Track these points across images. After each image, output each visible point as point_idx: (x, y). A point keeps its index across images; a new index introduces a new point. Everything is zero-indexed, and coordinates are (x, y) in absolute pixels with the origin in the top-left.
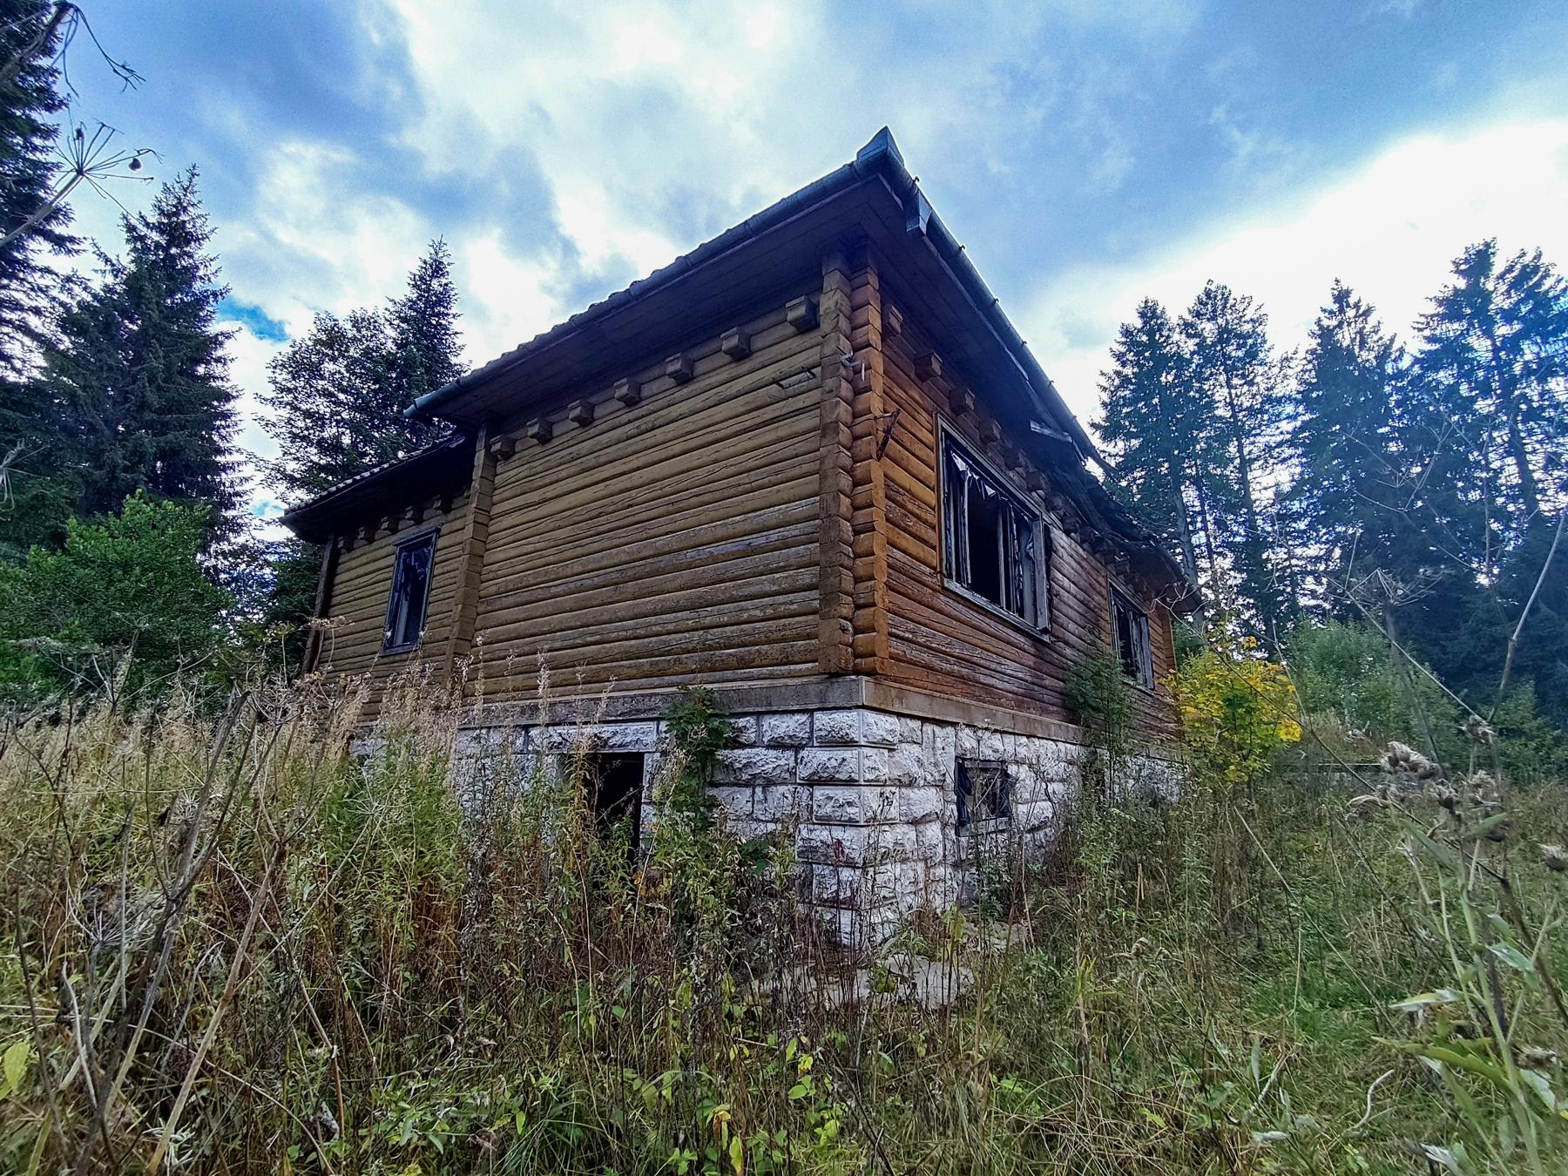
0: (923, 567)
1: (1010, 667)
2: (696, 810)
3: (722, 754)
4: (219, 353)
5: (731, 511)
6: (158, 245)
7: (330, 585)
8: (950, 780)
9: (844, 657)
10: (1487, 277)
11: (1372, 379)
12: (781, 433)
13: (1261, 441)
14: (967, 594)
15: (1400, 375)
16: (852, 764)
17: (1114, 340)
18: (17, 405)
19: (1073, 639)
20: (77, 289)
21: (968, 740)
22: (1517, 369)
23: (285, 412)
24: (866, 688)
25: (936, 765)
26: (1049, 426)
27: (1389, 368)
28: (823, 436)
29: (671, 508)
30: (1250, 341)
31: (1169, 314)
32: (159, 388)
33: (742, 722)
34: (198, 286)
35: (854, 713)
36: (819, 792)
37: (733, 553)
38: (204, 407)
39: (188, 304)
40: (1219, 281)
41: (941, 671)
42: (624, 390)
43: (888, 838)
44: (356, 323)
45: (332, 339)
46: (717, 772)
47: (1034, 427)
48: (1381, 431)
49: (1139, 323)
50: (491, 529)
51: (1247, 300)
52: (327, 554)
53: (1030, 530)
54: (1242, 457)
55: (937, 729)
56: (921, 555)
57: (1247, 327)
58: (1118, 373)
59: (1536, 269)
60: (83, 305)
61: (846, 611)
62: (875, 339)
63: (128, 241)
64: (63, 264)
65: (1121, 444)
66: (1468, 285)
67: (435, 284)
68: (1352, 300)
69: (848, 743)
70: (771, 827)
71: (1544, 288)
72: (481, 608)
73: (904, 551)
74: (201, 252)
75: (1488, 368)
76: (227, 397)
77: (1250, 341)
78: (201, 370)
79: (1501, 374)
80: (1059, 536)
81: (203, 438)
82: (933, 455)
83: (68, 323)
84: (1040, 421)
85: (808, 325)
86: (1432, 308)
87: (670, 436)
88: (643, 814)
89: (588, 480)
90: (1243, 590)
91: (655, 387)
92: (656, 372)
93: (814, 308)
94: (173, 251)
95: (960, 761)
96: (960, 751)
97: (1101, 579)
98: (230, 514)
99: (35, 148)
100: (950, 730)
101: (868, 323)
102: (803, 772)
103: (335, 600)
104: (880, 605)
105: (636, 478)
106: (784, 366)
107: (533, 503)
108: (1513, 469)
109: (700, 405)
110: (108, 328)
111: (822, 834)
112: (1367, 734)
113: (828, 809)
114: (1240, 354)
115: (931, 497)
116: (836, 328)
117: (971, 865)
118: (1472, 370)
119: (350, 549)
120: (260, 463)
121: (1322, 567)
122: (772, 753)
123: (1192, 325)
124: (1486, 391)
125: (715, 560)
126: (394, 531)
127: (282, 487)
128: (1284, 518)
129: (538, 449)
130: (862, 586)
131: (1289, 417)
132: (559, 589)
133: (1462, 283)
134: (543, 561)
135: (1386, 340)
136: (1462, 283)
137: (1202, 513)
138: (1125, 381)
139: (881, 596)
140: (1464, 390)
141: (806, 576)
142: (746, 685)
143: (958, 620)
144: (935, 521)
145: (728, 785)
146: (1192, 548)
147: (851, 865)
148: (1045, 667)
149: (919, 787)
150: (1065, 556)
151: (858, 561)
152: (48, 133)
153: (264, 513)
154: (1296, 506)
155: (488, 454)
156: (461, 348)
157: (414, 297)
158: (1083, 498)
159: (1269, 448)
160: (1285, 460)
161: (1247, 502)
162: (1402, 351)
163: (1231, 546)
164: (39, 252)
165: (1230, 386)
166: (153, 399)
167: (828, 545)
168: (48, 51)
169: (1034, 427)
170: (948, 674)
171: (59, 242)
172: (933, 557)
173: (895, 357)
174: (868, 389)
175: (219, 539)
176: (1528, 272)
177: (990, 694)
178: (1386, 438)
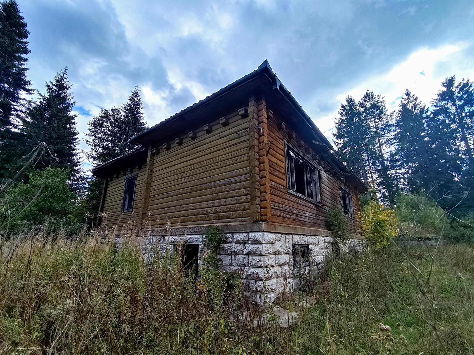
0: (281, 186)
1: (309, 214)
2: (214, 263)
3: (222, 245)
4: (73, 121)
5: (224, 171)
7: (106, 191)
8: (291, 251)
9: (258, 216)
10: (452, 87)
11: (418, 118)
12: (237, 148)
13: (385, 138)
14: (295, 194)
15: (427, 117)
17: (339, 109)
18: (15, 139)
19: (328, 204)
20: (33, 104)
21: (296, 238)
22: (464, 114)
23: (92, 138)
24: (264, 225)
25: (286, 247)
26: (318, 141)
27: (424, 115)
28: (250, 150)
29: (206, 170)
30: (381, 108)
32: (56, 132)
33: (228, 235)
34: (68, 101)
35: (261, 233)
36: (251, 258)
37: (224, 184)
38: (69, 137)
39: (65, 107)
40: (371, 90)
41: (287, 218)
42: (191, 135)
43: (272, 270)
44: (113, 111)
45: (106, 116)
46: (220, 251)
47: (314, 142)
48: (422, 134)
49: (346, 104)
50: (153, 176)
52: (105, 182)
53: (314, 172)
55: (286, 236)
56: (281, 183)
57: (380, 104)
58: (341, 119)
59: (468, 84)
60: (34, 108)
61: (258, 202)
62: (265, 120)
63: (47, 90)
64: (29, 97)
65: (342, 140)
66: (447, 90)
67: (136, 99)
68: (411, 95)
69: (259, 242)
70: (237, 268)
71: (471, 90)
72: (150, 199)
73: (275, 182)
74: (68, 92)
75: (454, 115)
76: (76, 134)
77: (381, 108)
78: (68, 126)
79: (458, 116)
80: (323, 174)
81: (68, 146)
82: (283, 152)
83: (30, 114)
84: (315, 140)
85: (245, 116)
86: (436, 97)
87: (205, 148)
88: (199, 263)
89: (181, 161)
90: (382, 183)
91: (200, 134)
92: (201, 129)
93: (246, 111)
94: (60, 92)
95: (294, 245)
96: (294, 242)
97: (336, 185)
98: (76, 168)
100: (290, 236)
101: (263, 115)
102: (246, 251)
103: (107, 196)
104: (268, 200)
105: (195, 161)
106: (238, 128)
107: (166, 167)
108: (464, 145)
109: (214, 139)
110: (41, 115)
111: (252, 270)
112: (422, 228)
113: (253, 263)
115: (283, 165)
116: (253, 117)
117: (298, 277)
118: (449, 115)
119: (111, 180)
120: (85, 153)
121: (406, 176)
122: (237, 245)
123: (362, 104)
124: (454, 121)
125: (219, 186)
126: (124, 175)
127: (91, 160)
128: (393, 162)
129: (166, 152)
130: (262, 194)
132: (174, 193)
133: (445, 89)
134: (168, 185)
135: (422, 107)
136: (445, 89)
138: (343, 121)
139: (268, 197)
140: (447, 121)
141: (246, 191)
142: (228, 224)
143: (292, 201)
144: (285, 172)
145: (224, 254)
146: (366, 171)
147: (261, 280)
148: (320, 213)
150: (325, 179)
151: (261, 187)
152: (26, 60)
153: (86, 166)
154: (397, 158)
155: (152, 153)
156: (144, 117)
157: (130, 103)
158: (330, 161)
159: (388, 141)
161: (382, 157)
162: (427, 110)
163: (378, 170)
164: (22, 94)
165: (375, 122)
166: (54, 135)
167: (253, 183)
169: (314, 142)
170: (290, 218)
171: (28, 91)
172: (284, 183)
174: (263, 135)
175: (73, 176)
176: (465, 85)
177: (303, 224)
178: (424, 136)
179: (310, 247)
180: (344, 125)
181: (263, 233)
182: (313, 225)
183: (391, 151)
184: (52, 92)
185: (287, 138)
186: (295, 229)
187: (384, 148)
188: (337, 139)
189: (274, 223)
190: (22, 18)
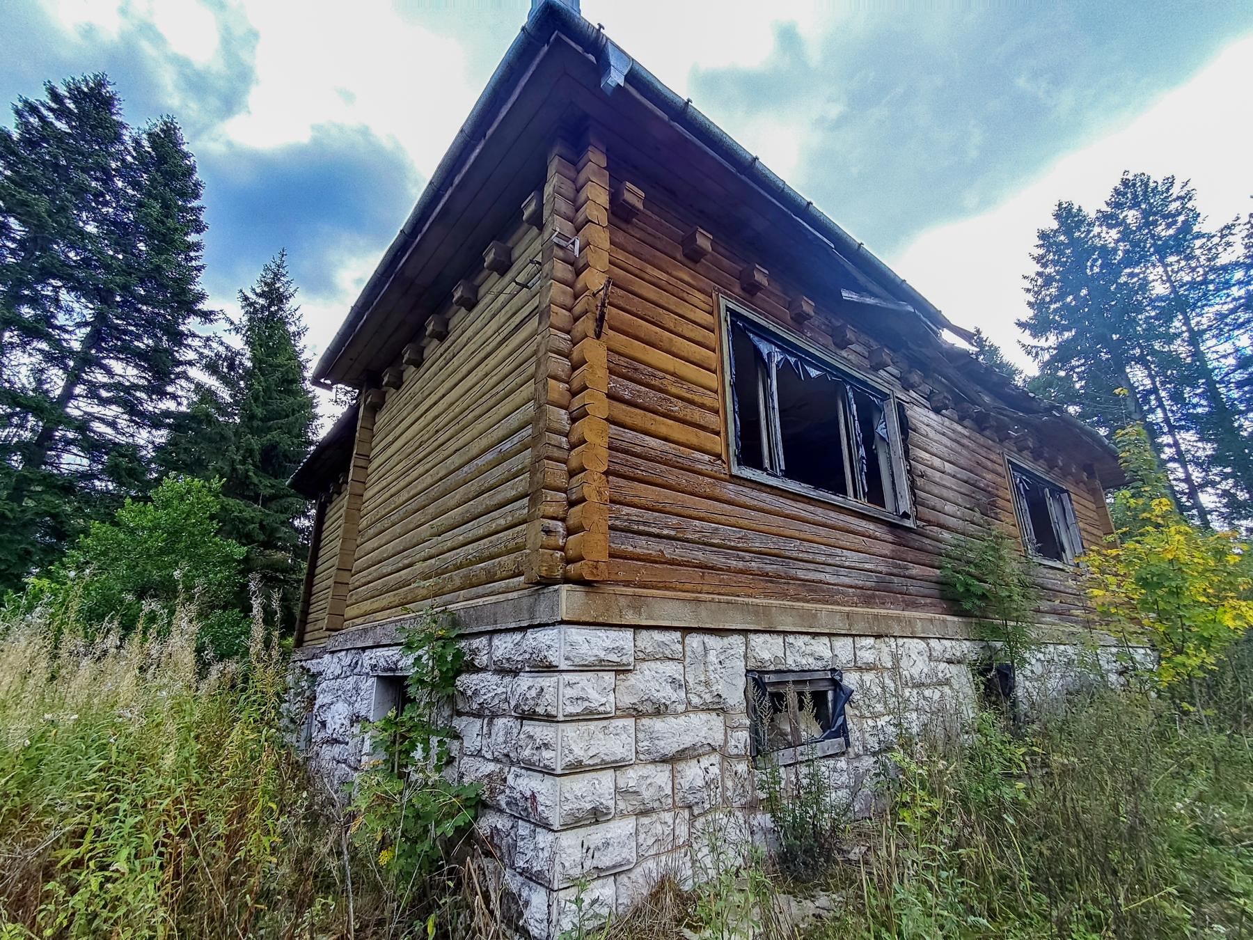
0: (698, 455)
6: (263, 306)
16: (548, 696)
17: (1032, 244)
19: (951, 522)
24: (567, 599)
25: (707, 684)
30: (1181, 218)
31: (1085, 211)
33: (476, 643)
36: (530, 727)
41: (729, 570)
47: (846, 294)
49: (1055, 225)
51: (1170, 181)
54: (1190, 330)
58: (1039, 274)
64: (204, 330)
73: (665, 439)
77: (1181, 218)
80: (921, 416)
90: (1213, 460)
94: (273, 309)
99: (192, 259)
100: (737, 640)
104: (593, 498)
114: (1171, 232)
131: (1239, 282)
137: (1154, 391)
138: (1048, 281)
142: (480, 601)
143: (771, 507)
147: (547, 827)
148: (911, 555)
149: (676, 714)
150: (932, 434)
158: (951, 372)
159: (1221, 317)
160: (1243, 324)
165: (1165, 266)
168: (197, 196)
171: (207, 316)
173: (650, 239)
177: (816, 591)
179: (850, 680)
180: (1053, 291)
181: (563, 627)
182: (873, 597)
183: (1237, 350)
184: (256, 311)
185: (737, 290)
186: (756, 610)
187: (1209, 343)
188: (1034, 336)
189: (630, 591)
190: (186, 156)
